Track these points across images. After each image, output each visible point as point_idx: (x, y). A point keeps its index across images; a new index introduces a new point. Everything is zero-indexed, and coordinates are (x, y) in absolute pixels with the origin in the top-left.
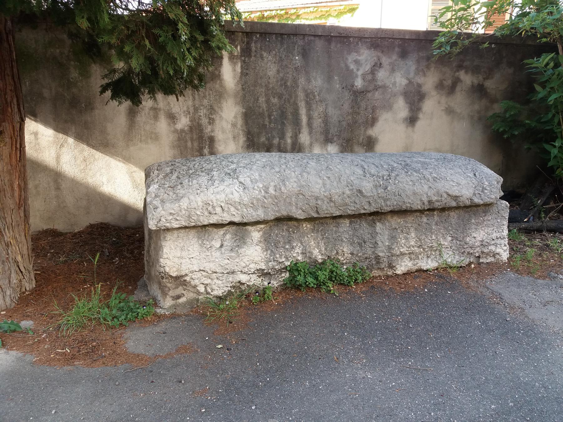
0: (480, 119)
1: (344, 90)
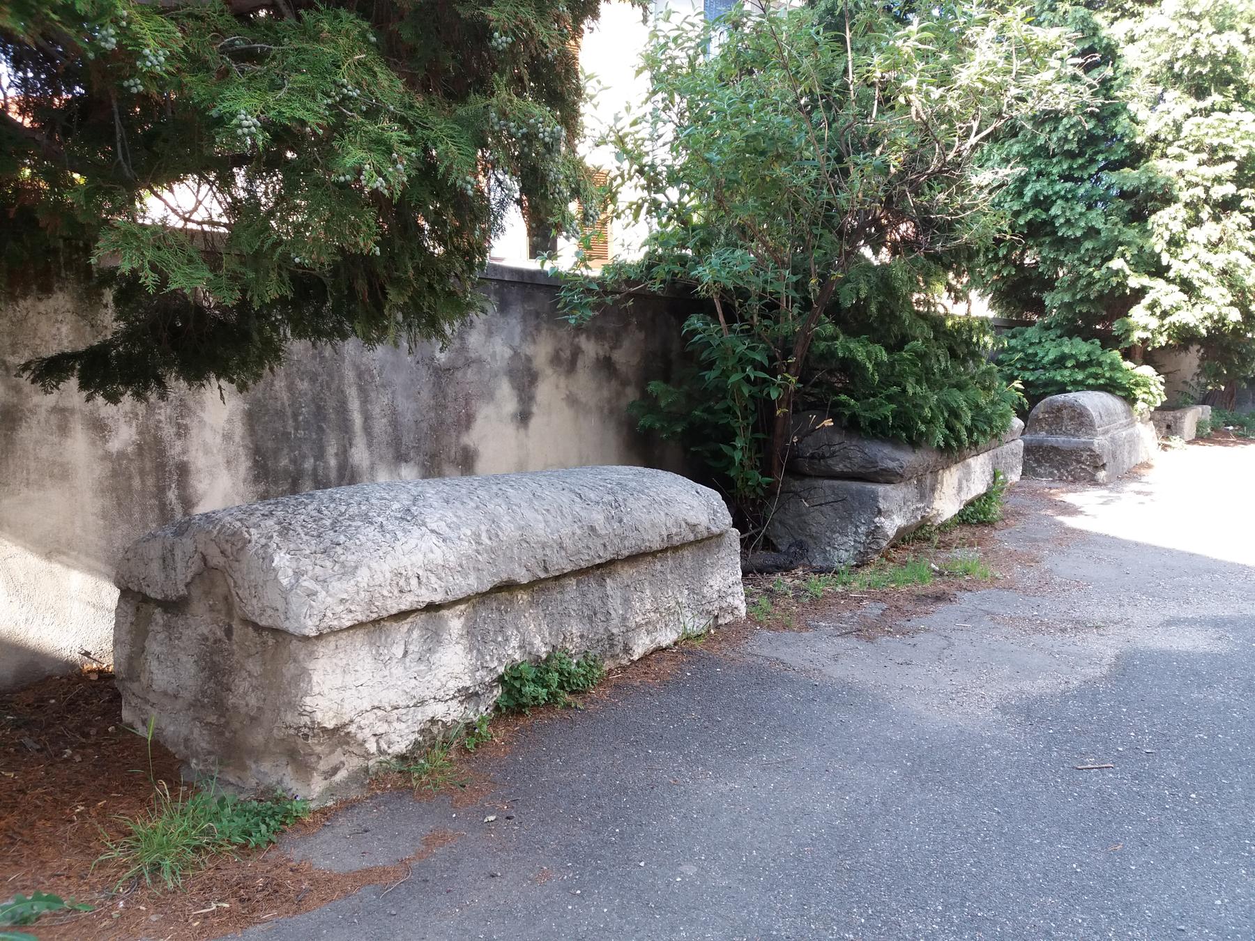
0: (611, 411)
1: (420, 366)
